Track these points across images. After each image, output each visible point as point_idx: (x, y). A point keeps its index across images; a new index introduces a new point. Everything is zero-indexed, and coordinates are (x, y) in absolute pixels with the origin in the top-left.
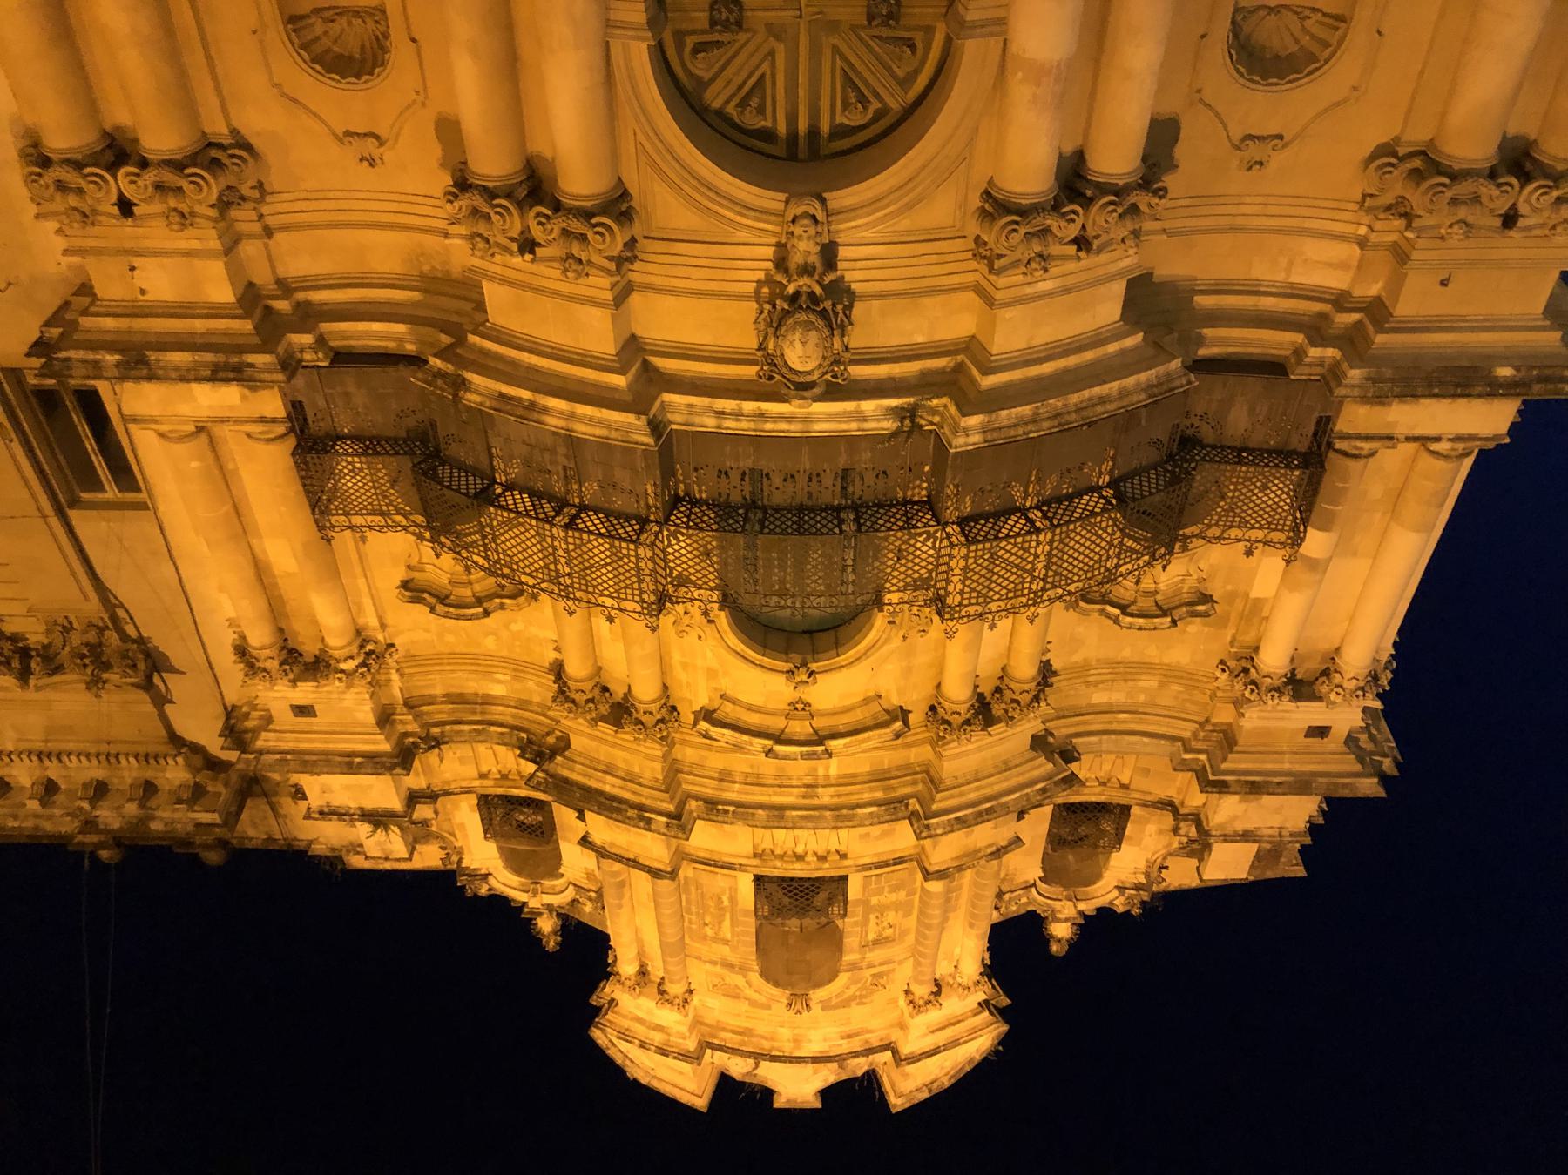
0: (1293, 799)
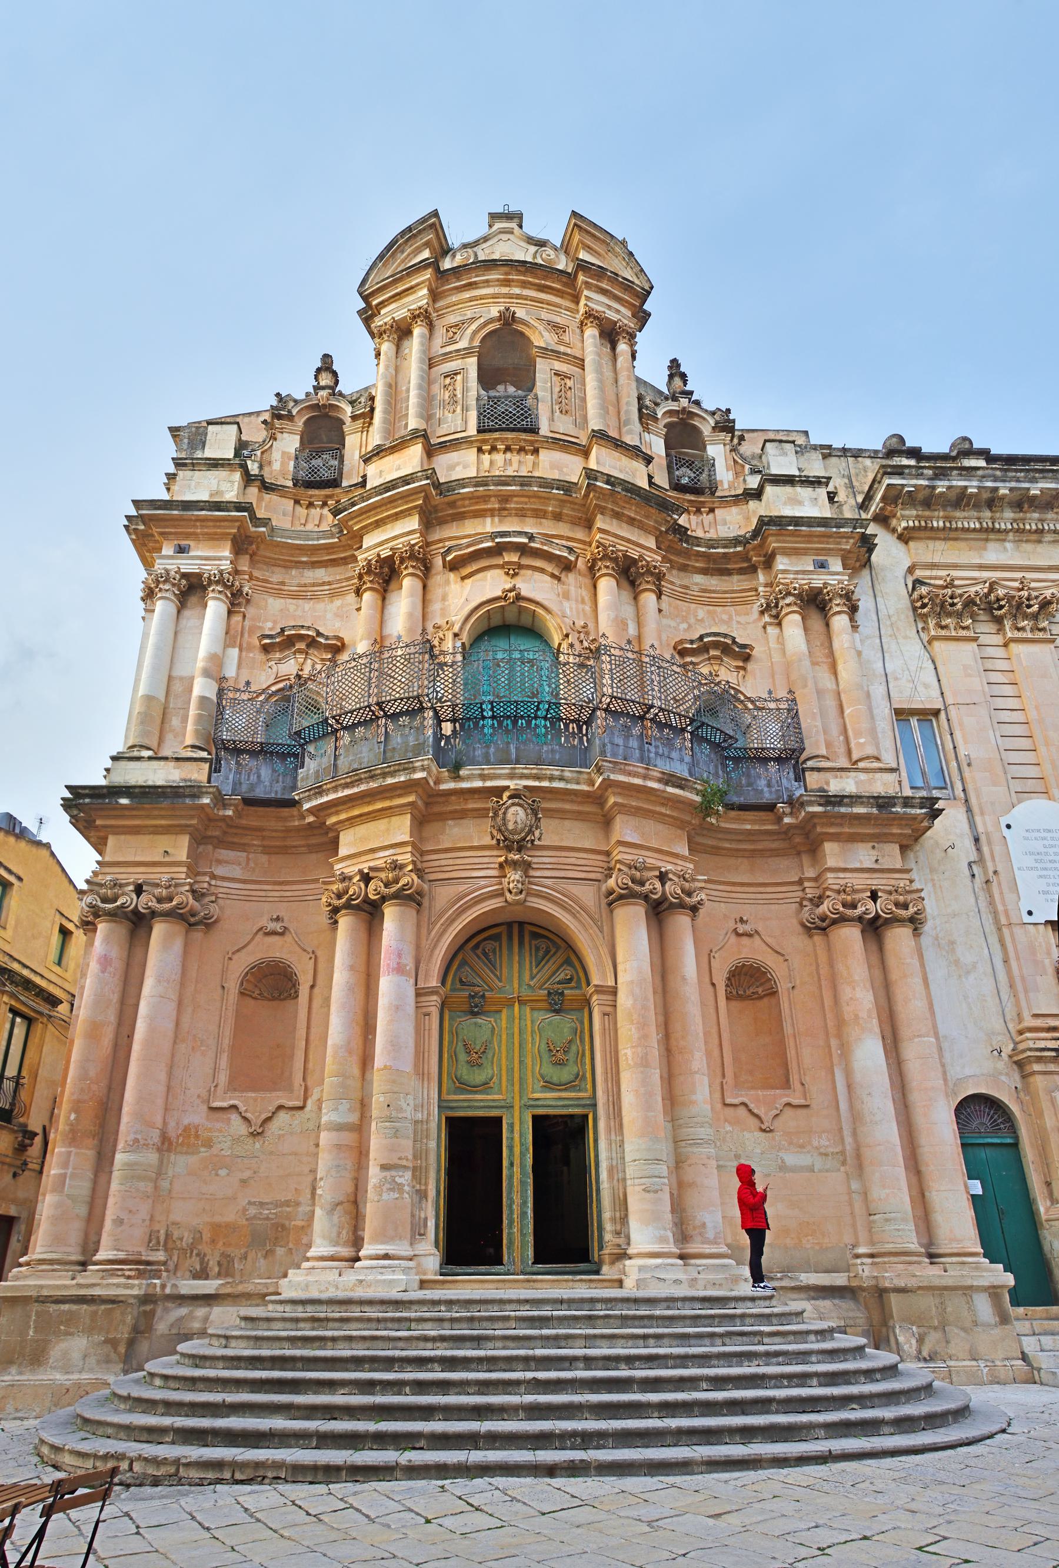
0: (411, 1152)
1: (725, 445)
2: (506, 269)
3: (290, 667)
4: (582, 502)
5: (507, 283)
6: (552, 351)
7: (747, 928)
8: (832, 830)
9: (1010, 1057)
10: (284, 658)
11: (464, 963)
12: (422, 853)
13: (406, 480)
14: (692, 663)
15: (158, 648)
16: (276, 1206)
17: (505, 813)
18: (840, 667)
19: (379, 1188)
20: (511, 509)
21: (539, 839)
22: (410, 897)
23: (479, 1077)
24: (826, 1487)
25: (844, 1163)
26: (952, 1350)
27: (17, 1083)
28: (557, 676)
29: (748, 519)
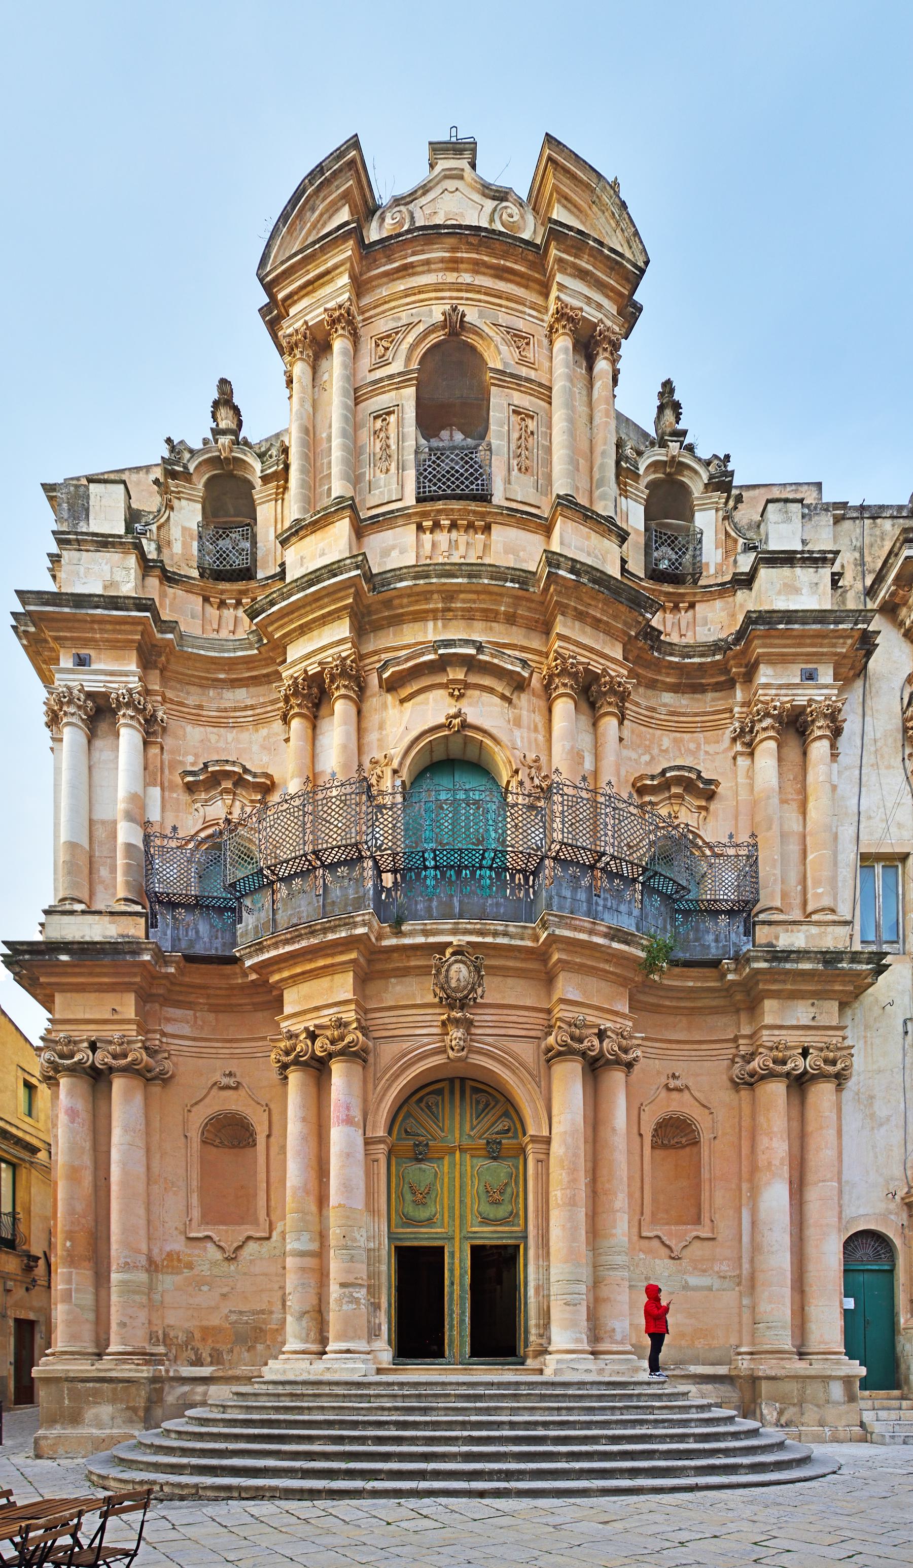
1: (717, 510)
2: (451, 241)
3: (217, 810)
4: (541, 599)
5: (453, 265)
6: (512, 375)
7: (678, 1083)
8: (774, 987)
9: (903, 1199)
10: (210, 799)
11: (409, 1115)
12: (366, 1011)
13: (332, 570)
14: (650, 803)
15: (73, 787)
16: (254, 1314)
17: (447, 971)
18: (811, 805)
19: (340, 1301)
20: (456, 609)
21: (482, 997)
22: (355, 1054)
23: (423, 1214)
24: (690, 1506)
25: (739, 1284)
26: (805, 1419)
27: (14, 1218)
28: (505, 819)
29: (733, 615)
